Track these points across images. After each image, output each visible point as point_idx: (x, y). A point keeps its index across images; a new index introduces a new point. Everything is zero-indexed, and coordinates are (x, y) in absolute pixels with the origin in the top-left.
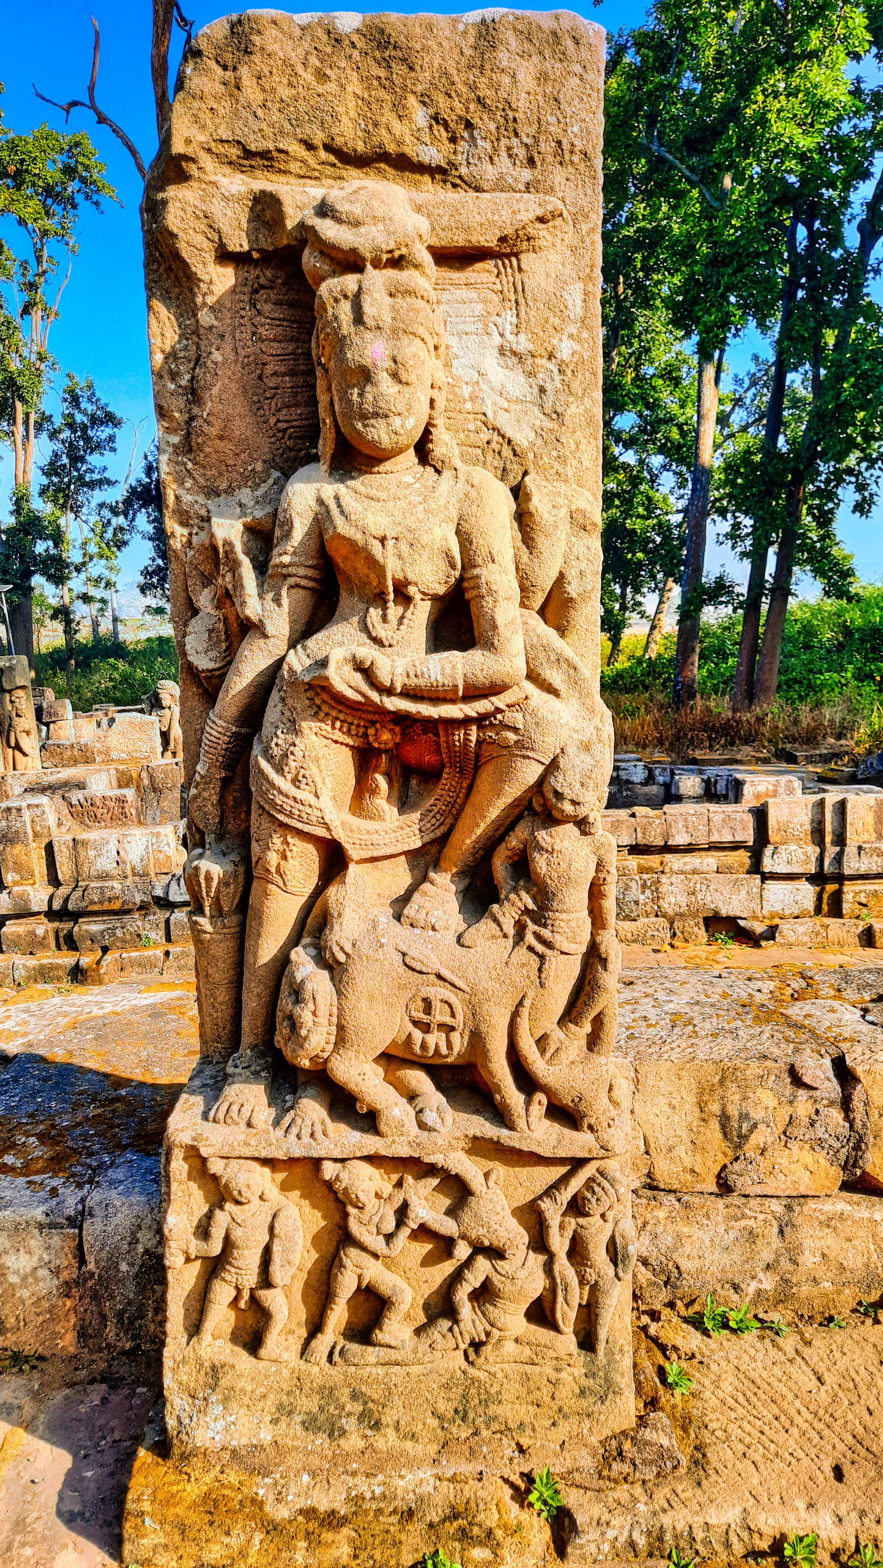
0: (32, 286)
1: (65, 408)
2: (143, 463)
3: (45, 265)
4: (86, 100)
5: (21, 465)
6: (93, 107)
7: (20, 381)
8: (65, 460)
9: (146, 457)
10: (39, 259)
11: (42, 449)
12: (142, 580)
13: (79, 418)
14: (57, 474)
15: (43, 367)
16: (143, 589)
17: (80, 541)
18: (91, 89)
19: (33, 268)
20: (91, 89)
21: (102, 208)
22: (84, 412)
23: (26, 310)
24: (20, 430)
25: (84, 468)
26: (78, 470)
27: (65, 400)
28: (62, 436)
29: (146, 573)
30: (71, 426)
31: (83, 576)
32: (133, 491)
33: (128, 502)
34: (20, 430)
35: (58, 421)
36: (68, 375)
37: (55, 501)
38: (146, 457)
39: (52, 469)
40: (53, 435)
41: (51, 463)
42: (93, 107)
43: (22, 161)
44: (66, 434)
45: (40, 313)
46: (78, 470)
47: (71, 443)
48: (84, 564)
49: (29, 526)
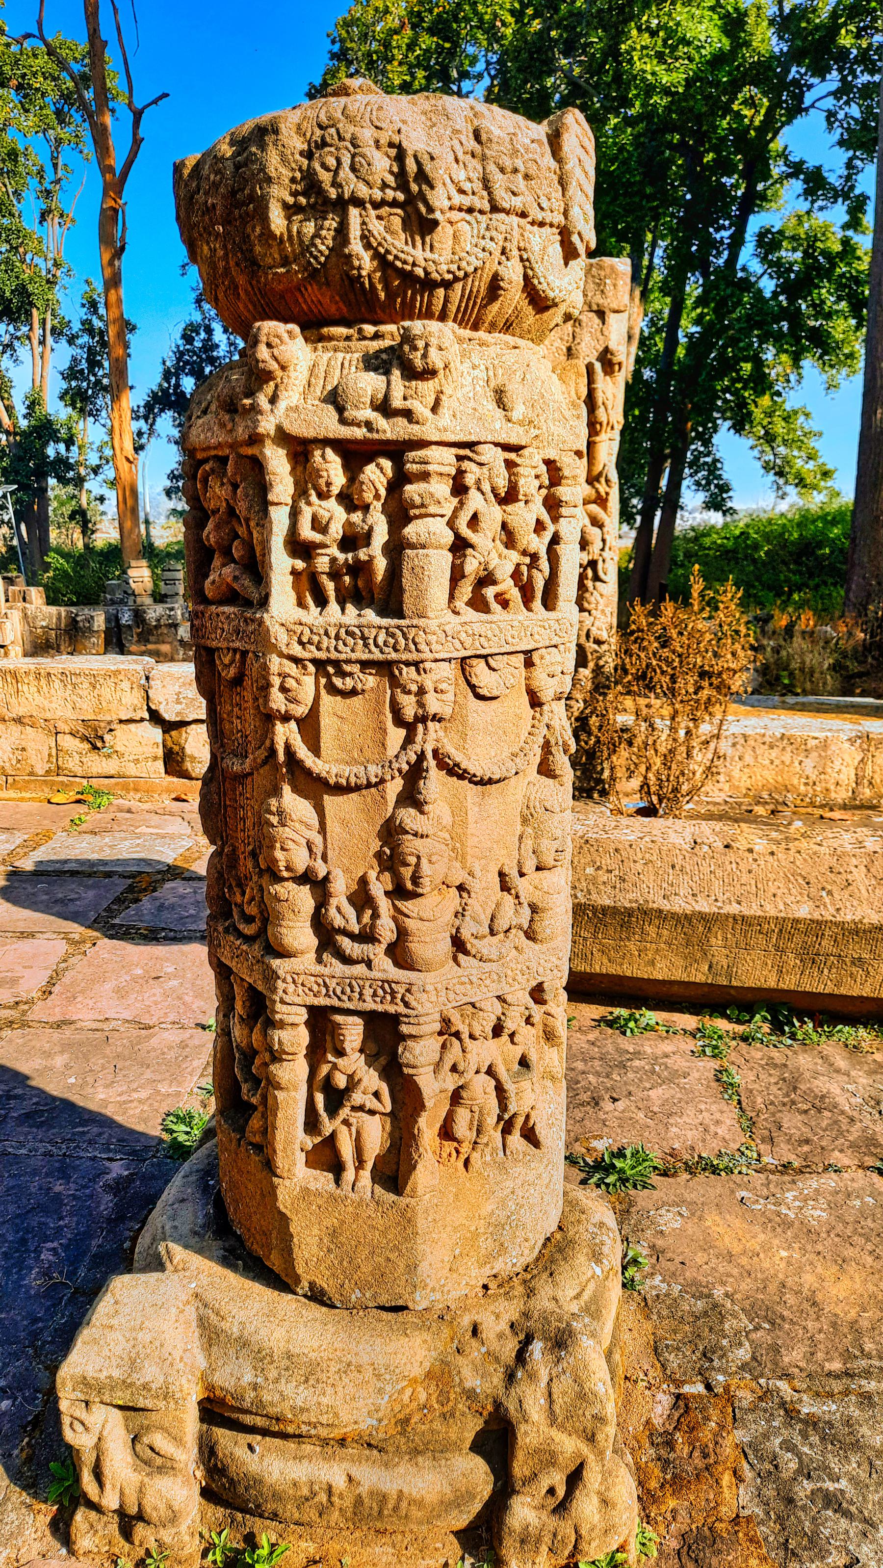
0: (48, 193)
1: (83, 313)
2: (161, 369)
3: (60, 173)
4: (37, 33)
5: (38, 370)
6: (42, 38)
7: (30, 288)
8: (84, 365)
9: (164, 363)
10: (55, 166)
11: (62, 355)
12: (168, 483)
13: (97, 323)
14: (76, 379)
15: (59, 273)
16: (168, 493)
17: (98, 444)
18: (40, 23)
19: (49, 175)
20: (40, 23)
21: (117, 115)
22: (100, 318)
23: (44, 216)
24: (37, 332)
25: (100, 373)
26: (95, 375)
27: (83, 305)
28: (80, 341)
29: (172, 476)
30: (89, 330)
31: (100, 478)
32: (154, 395)
33: (149, 407)
34: (37, 332)
35: (76, 326)
36: (87, 281)
37: (73, 405)
38: (164, 363)
39: (71, 374)
40: (71, 341)
41: (71, 368)
42: (42, 38)
43: (24, 76)
44: (85, 339)
45: (56, 220)
46: (95, 375)
47: (90, 348)
48: (99, 467)
49: (45, 430)
